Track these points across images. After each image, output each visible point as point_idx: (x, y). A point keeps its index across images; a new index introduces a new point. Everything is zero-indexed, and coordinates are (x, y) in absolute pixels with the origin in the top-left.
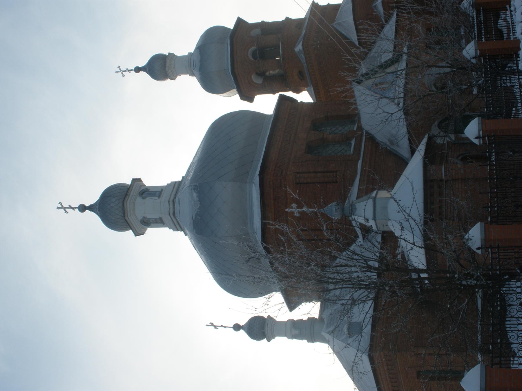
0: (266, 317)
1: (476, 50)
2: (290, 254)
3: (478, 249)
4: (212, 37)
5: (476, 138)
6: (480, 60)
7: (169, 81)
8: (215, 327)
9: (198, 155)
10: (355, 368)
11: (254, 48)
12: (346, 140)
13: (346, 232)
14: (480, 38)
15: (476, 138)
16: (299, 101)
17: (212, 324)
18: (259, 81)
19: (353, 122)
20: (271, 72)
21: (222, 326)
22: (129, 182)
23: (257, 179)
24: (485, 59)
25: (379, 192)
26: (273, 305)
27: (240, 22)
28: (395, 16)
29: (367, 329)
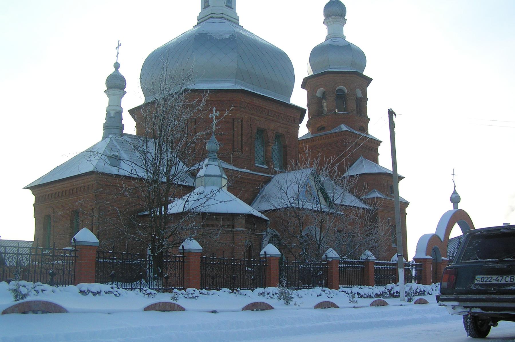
0: (125, 90)
1: (332, 258)
2: (183, 107)
3: (183, 247)
4: (359, 57)
5: (265, 252)
6: (324, 261)
7: (323, 18)
8: (117, 48)
9: (260, 40)
10: (92, 153)
11: (346, 91)
12: (267, 161)
13: (195, 155)
14: (340, 262)
15: (265, 252)
16: (300, 125)
17: (120, 45)
18: (319, 94)
19: (281, 168)
20: (325, 104)
21: (118, 53)
22: (345, 18)
23: (238, 87)
24: (324, 264)
25: (226, 181)
26: (134, 97)
27: (369, 80)
28: (364, 206)
29: (114, 171)
